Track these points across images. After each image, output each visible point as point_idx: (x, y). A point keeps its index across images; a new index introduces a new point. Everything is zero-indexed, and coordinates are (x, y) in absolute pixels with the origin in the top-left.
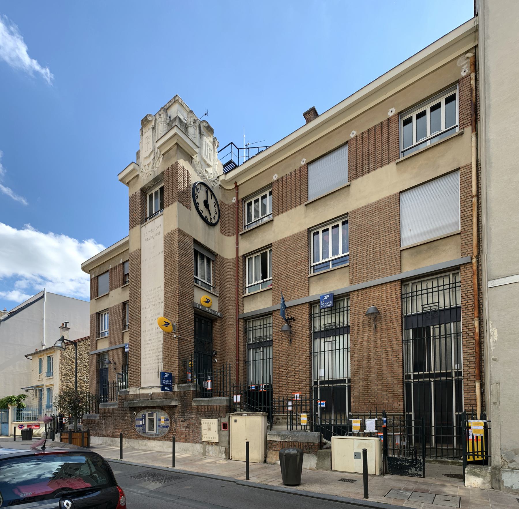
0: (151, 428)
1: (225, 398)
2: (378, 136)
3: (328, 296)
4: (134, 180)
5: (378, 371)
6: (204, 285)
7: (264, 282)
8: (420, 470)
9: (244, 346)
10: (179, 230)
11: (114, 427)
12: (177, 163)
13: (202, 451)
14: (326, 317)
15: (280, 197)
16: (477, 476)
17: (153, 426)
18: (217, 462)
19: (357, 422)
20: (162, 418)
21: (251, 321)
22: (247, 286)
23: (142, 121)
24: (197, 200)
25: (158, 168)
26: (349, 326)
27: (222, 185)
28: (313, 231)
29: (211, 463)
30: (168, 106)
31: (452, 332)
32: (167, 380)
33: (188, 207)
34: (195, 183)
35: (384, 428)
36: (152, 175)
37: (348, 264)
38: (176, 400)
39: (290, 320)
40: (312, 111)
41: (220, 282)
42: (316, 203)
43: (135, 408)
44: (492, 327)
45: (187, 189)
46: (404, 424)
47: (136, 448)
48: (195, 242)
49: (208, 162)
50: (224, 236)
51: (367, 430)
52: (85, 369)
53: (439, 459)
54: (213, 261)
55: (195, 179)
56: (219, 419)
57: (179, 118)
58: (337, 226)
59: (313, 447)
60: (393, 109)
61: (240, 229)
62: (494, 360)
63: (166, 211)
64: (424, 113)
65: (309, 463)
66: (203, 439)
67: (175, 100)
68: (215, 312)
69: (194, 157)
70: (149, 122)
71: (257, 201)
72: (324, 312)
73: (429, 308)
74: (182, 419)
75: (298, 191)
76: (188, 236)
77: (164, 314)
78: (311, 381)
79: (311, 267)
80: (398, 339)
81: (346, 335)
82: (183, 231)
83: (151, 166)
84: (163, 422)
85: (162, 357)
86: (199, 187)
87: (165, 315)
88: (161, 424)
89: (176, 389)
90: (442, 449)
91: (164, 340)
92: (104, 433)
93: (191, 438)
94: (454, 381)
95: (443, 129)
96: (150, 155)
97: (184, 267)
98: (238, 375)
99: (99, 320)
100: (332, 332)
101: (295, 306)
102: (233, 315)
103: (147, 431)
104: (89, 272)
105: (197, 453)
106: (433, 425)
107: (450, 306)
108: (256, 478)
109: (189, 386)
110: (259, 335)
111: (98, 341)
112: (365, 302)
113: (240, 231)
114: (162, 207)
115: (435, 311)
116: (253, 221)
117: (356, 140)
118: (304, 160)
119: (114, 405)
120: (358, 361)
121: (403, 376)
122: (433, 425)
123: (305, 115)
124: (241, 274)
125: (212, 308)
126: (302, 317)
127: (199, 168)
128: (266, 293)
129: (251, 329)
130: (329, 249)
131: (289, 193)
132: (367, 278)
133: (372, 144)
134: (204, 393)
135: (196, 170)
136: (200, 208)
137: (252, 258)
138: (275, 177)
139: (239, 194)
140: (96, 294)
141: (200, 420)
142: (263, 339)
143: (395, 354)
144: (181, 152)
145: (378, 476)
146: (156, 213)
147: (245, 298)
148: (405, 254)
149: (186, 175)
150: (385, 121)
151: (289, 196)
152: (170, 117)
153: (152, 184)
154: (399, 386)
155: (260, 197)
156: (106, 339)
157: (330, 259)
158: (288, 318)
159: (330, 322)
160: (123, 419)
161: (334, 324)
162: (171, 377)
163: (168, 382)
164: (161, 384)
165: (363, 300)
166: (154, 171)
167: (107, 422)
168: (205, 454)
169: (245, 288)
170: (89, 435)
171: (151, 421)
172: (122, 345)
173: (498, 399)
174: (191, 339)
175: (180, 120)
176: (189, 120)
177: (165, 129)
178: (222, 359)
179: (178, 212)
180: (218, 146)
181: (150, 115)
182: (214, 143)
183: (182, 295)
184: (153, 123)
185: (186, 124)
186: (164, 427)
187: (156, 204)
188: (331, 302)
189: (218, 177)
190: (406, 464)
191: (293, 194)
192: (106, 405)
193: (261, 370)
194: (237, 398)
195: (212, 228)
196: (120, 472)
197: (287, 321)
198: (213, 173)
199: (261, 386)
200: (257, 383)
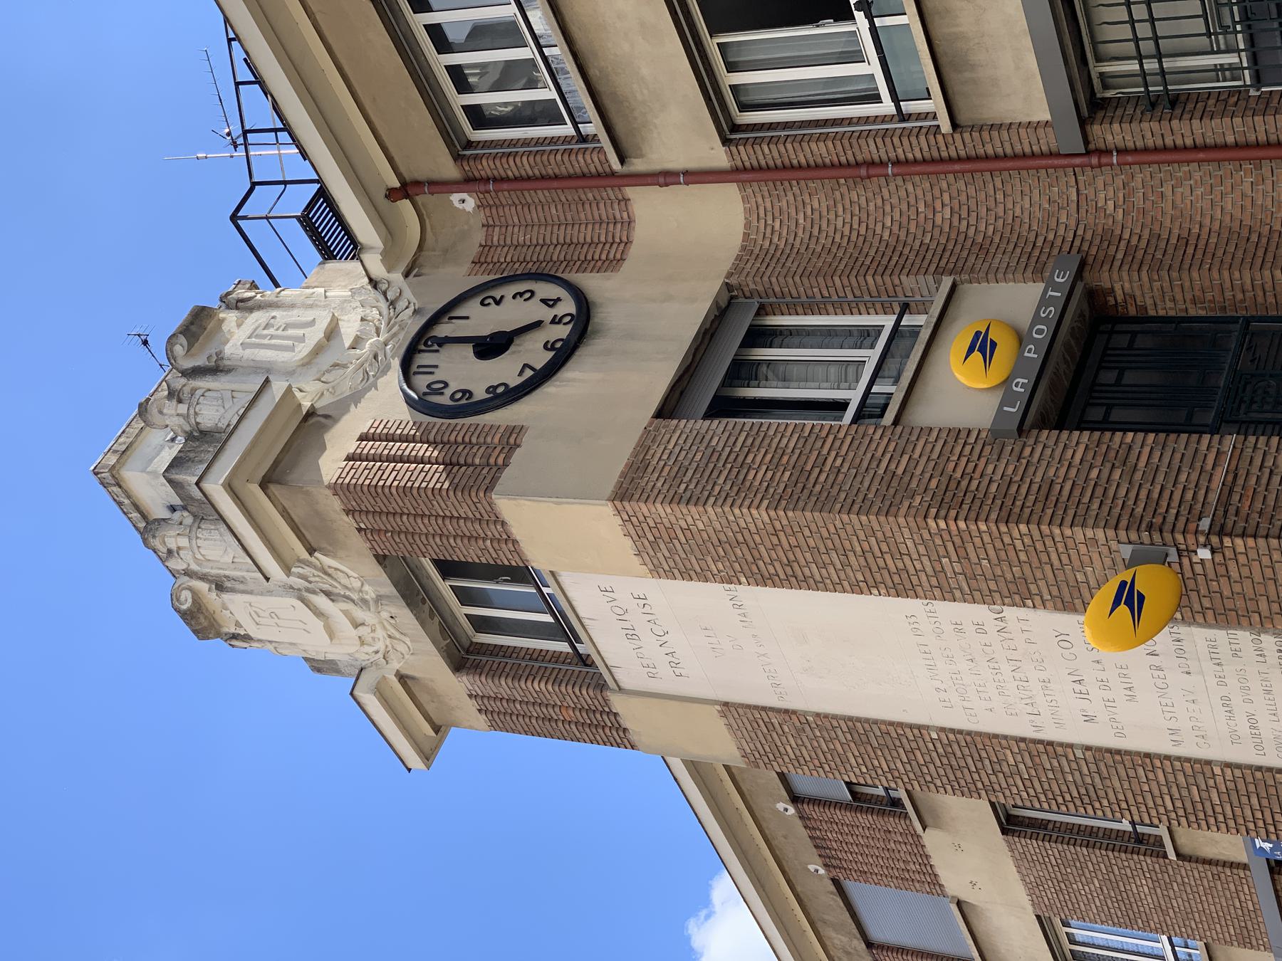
4: (423, 698)
6: (892, 365)
10: (622, 495)
21: (1096, 69)
24: (480, 394)
27: (403, 267)
30: (135, 515)
33: (512, 439)
41: (874, 269)
45: (434, 443)
49: (315, 335)
50: (633, 250)
54: (762, 310)
55: (387, 403)
57: (172, 466)
61: (594, 165)
67: (111, 480)
68: (1044, 301)
69: (306, 404)
76: (643, 448)
77: (1067, 606)
82: (624, 475)
83: (359, 614)
86: (422, 381)
87: (1071, 602)
96: (318, 613)
97: (801, 474)
111: (1186, 849)
114: (521, 574)
116: (552, 94)
124: (822, 151)
125: (1024, 320)
127: (347, 382)
135: (356, 397)
136: (514, 381)
137: (735, 89)
146: (548, 604)
147: (962, 118)
149: (380, 447)
152: (173, 509)
166: (379, 599)
169: (902, 117)
175: (176, 463)
176: (175, 422)
180: (254, 286)
181: (175, 598)
182: (242, 306)
183: (953, 499)
185: (190, 437)
189: (374, 283)
195: (599, 317)
198: (360, 312)
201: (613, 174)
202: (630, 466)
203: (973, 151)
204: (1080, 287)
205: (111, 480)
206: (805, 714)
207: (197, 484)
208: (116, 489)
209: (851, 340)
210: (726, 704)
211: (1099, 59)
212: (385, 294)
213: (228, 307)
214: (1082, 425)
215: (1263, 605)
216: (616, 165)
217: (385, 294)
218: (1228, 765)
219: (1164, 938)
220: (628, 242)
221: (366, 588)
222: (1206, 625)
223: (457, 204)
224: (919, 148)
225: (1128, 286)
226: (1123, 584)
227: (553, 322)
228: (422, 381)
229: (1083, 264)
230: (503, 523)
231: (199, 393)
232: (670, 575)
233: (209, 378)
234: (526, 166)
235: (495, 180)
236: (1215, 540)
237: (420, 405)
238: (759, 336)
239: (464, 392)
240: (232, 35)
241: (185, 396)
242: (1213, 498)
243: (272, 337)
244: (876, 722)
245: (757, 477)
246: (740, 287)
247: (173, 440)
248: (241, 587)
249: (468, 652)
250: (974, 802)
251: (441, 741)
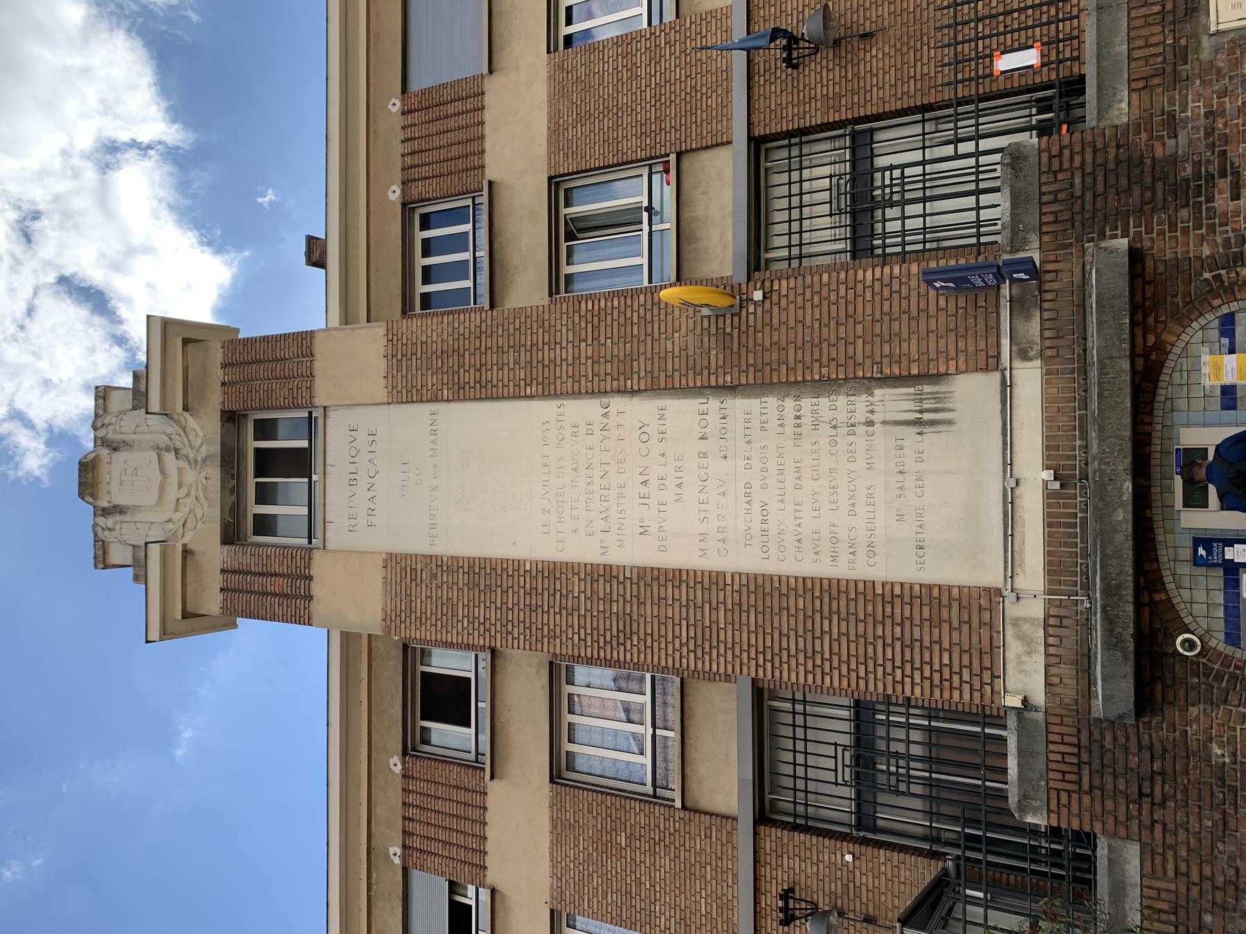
26: (857, 702)
28: (560, 770)
74: (1222, 201)
79: (655, 796)
128: (691, 703)
157: (650, 731)
207: (147, 413)
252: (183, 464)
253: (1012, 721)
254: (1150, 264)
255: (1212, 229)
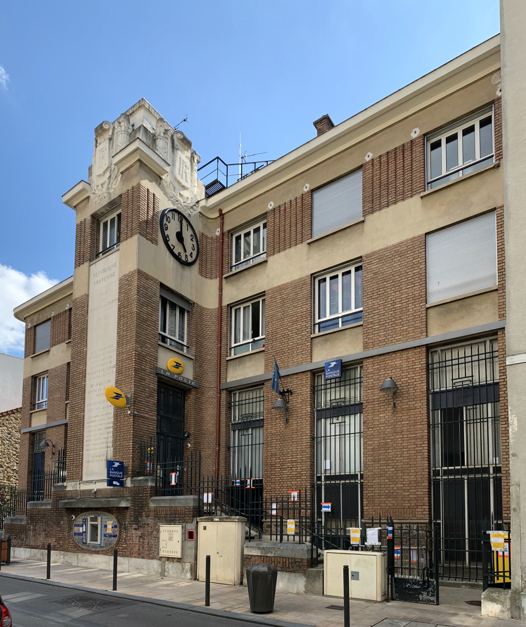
0: (94, 538)
1: (192, 497)
2: (399, 161)
3: (335, 363)
4: (83, 204)
5: (398, 464)
6: (173, 343)
7: (254, 341)
8: (432, 596)
9: (227, 426)
10: (139, 272)
11: (46, 534)
12: (139, 184)
13: (160, 570)
14: (333, 390)
15: (277, 232)
16: (495, 602)
17: (97, 536)
18: (176, 585)
19: (356, 531)
20: (109, 524)
21: (237, 392)
22: (233, 345)
23: (96, 130)
24: (167, 233)
25: (115, 189)
26: (362, 404)
27: (202, 212)
28: (317, 278)
29: (167, 585)
30: (131, 111)
31: (490, 416)
32: (116, 471)
33: (154, 241)
34: (165, 210)
35: (388, 540)
36: (107, 198)
37: (361, 323)
38: (127, 500)
39: (285, 394)
40: (326, 120)
41: (197, 340)
42: (322, 242)
43: (75, 508)
44: (512, 414)
45: (153, 217)
46: (431, 535)
47: (74, 564)
48: (163, 286)
49: (184, 183)
50: (204, 279)
51: (368, 543)
52: (15, 453)
53: (473, 582)
54: (188, 312)
55: (164, 204)
56: (184, 525)
57: (145, 128)
58: (349, 272)
59: (301, 564)
60: (417, 130)
61: (225, 270)
62: (514, 455)
63: (123, 245)
64: (454, 137)
65: (286, 585)
66: (162, 554)
67: (140, 105)
68: (188, 380)
69: (163, 177)
70: (105, 130)
71: (247, 235)
72: (331, 383)
73: (461, 384)
74: (134, 526)
75: (299, 226)
76: (152, 279)
77: (117, 382)
78: (312, 476)
80: (423, 423)
81: (359, 414)
82: (145, 273)
83: (105, 186)
84: (109, 530)
85: (111, 439)
86: (170, 215)
87: (118, 383)
88: (108, 532)
89: (129, 483)
90: (477, 569)
91: (114, 417)
92: (32, 543)
93: (146, 552)
94: (491, 480)
95: (478, 159)
96: (105, 172)
97: (145, 321)
98: (219, 465)
99: (35, 386)
100: (341, 410)
101: (293, 374)
102: (213, 384)
103: (88, 542)
104: (25, 320)
105: (153, 573)
106: (467, 537)
107: (486, 381)
108: (219, 604)
109: (147, 481)
110: (247, 413)
111: (33, 415)
112: (382, 372)
113: (225, 272)
114: (119, 241)
115: (468, 388)
116: (242, 261)
117: (373, 164)
118: (308, 185)
119: (46, 504)
120: (373, 450)
121: (429, 472)
122: (467, 537)
123: (316, 124)
124: (224, 329)
125: (183, 375)
126: (302, 389)
127: (169, 191)
128: (256, 356)
129: (237, 403)
130: (340, 301)
131: (287, 227)
132: (385, 342)
133: (395, 167)
134: (164, 489)
135: (166, 194)
136: (170, 243)
137: (240, 308)
138: (271, 206)
139: (225, 225)
140: (32, 350)
141: (159, 526)
142: (252, 417)
143: (419, 442)
144: (146, 171)
145: (380, 602)
146: (112, 246)
147: (229, 362)
148: (431, 312)
149: (151, 200)
150: (408, 143)
151: (288, 231)
152: (133, 126)
153: (107, 210)
154: (423, 484)
155: (251, 229)
156: (44, 412)
157: (340, 315)
158: (284, 390)
159: (338, 397)
160: (58, 524)
161: (343, 400)
162: (122, 468)
163: (118, 474)
164: (108, 476)
165: (379, 370)
166: (110, 194)
167: (37, 528)
168: (163, 574)
169: (230, 349)
170: (9, 546)
171: (95, 528)
172: (65, 421)
173: (518, 504)
174: (153, 416)
175: (146, 130)
176: (158, 131)
177: (125, 140)
178: (197, 444)
179: (139, 249)
180: (198, 162)
181: (106, 122)
182: (192, 158)
183: (140, 358)
184: (110, 133)
185: (154, 135)
186: (111, 536)
187: (111, 234)
188: (338, 371)
189: (198, 202)
190: (416, 587)
191: (293, 228)
192: (36, 505)
193: (250, 460)
194: (208, 498)
195: (187, 268)
196: (42, 595)
197: (282, 394)
198: (190, 197)
199: (249, 481)
200: (243, 476)
201: (222, 275)
202: (147, 275)
203: (222, 365)
204: (191, 387)
205: (140, 105)
206: (87, 317)
208: (138, 106)
209: (181, 334)
210: (88, 296)
211: (239, 393)
212: (195, 205)
213: (192, 153)
214: (158, 386)
215: (119, 424)
216: (224, 276)
217: (195, 205)
218: (84, 416)
219: (264, 337)
220: (206, 277)
221: (113, 190)
222: (114, 412)
223: (415, 130)
224: (223, 352)
225: (191, 397)
226: (121, 395)
227: (186, 255)
228: (170, 215)
229: (196, 388)
230: (131, 236)
231: (167, 140)
232: (120, 283)
233: (171, 145)
234: (226, 251)
235: (223, 242)
236: (132, 415)
237: (163, 214)
238: (182, 311)
239: (167, 228)
240: (269, 163)
241: (166, 136)
242: (142, 414)
243: (183, 168)
244: (87, 335)
245: (145, 309)
246: (194, 306)
247: (153, 129)
248: (111, 147)
249: (97, 220)
250: (70, 358)
251: (71, 208)
252: (107, 181)
253: (62, 484)
254: (126, 511)
255: (130, 524)
